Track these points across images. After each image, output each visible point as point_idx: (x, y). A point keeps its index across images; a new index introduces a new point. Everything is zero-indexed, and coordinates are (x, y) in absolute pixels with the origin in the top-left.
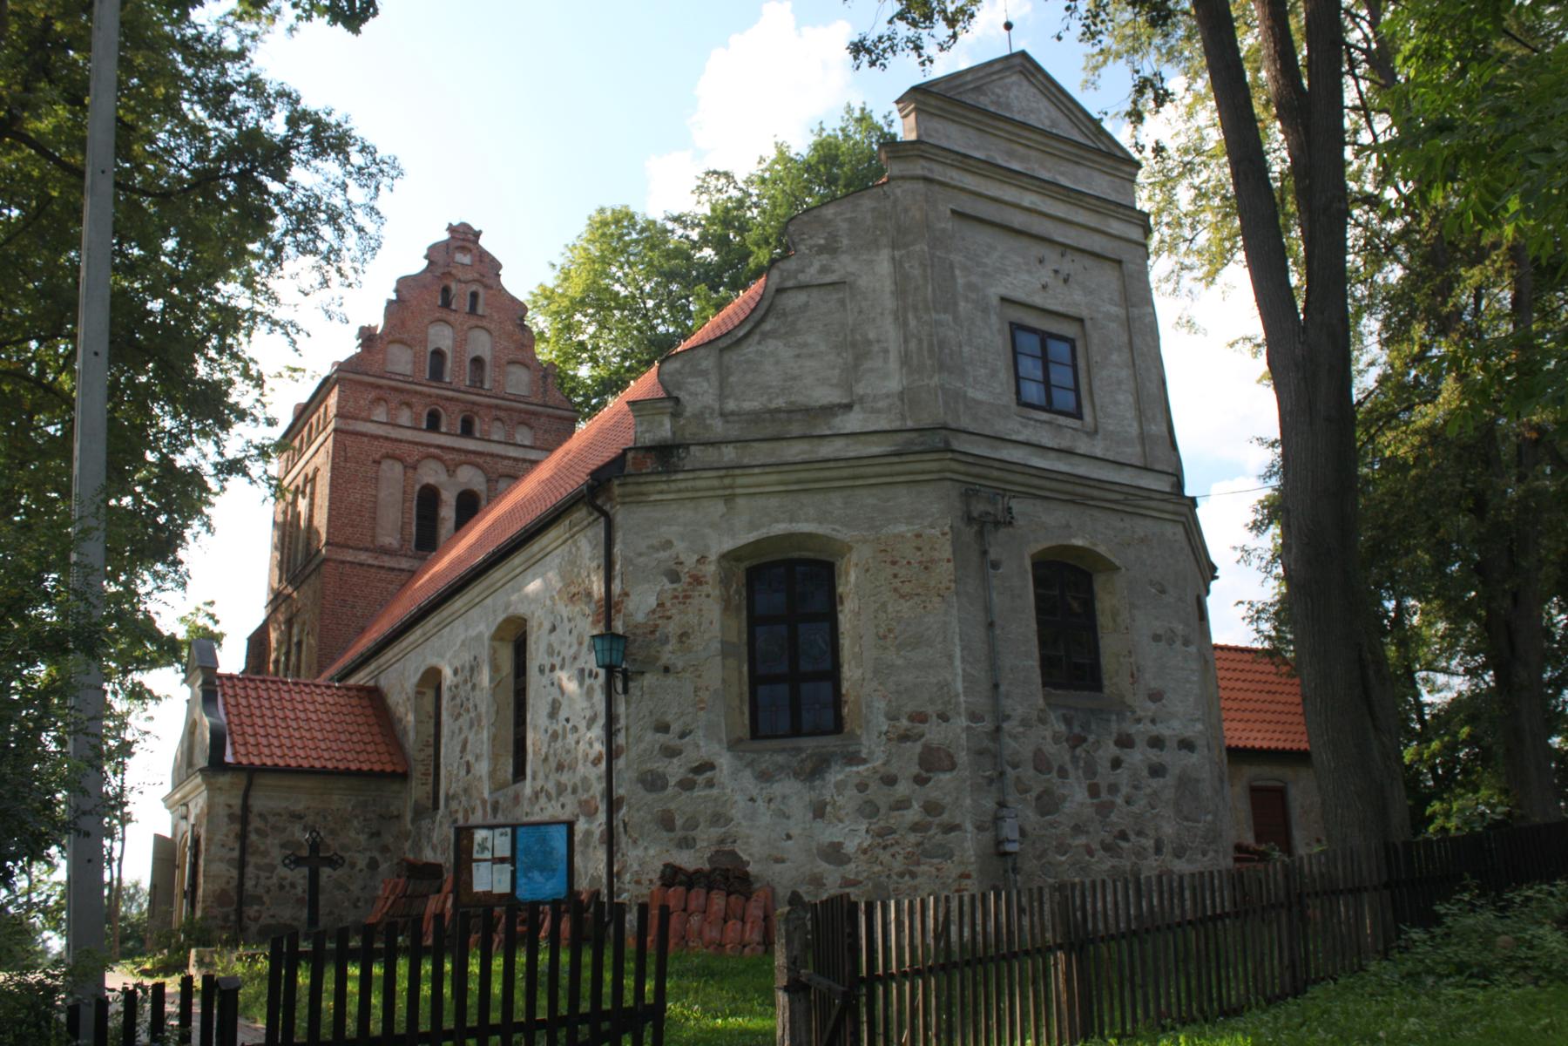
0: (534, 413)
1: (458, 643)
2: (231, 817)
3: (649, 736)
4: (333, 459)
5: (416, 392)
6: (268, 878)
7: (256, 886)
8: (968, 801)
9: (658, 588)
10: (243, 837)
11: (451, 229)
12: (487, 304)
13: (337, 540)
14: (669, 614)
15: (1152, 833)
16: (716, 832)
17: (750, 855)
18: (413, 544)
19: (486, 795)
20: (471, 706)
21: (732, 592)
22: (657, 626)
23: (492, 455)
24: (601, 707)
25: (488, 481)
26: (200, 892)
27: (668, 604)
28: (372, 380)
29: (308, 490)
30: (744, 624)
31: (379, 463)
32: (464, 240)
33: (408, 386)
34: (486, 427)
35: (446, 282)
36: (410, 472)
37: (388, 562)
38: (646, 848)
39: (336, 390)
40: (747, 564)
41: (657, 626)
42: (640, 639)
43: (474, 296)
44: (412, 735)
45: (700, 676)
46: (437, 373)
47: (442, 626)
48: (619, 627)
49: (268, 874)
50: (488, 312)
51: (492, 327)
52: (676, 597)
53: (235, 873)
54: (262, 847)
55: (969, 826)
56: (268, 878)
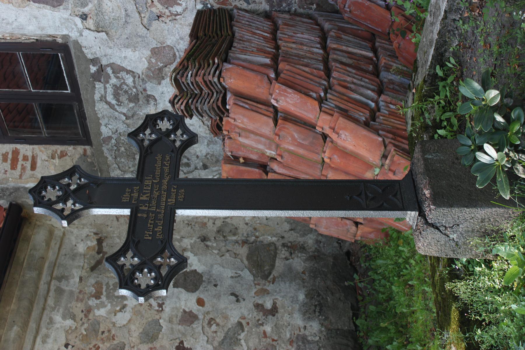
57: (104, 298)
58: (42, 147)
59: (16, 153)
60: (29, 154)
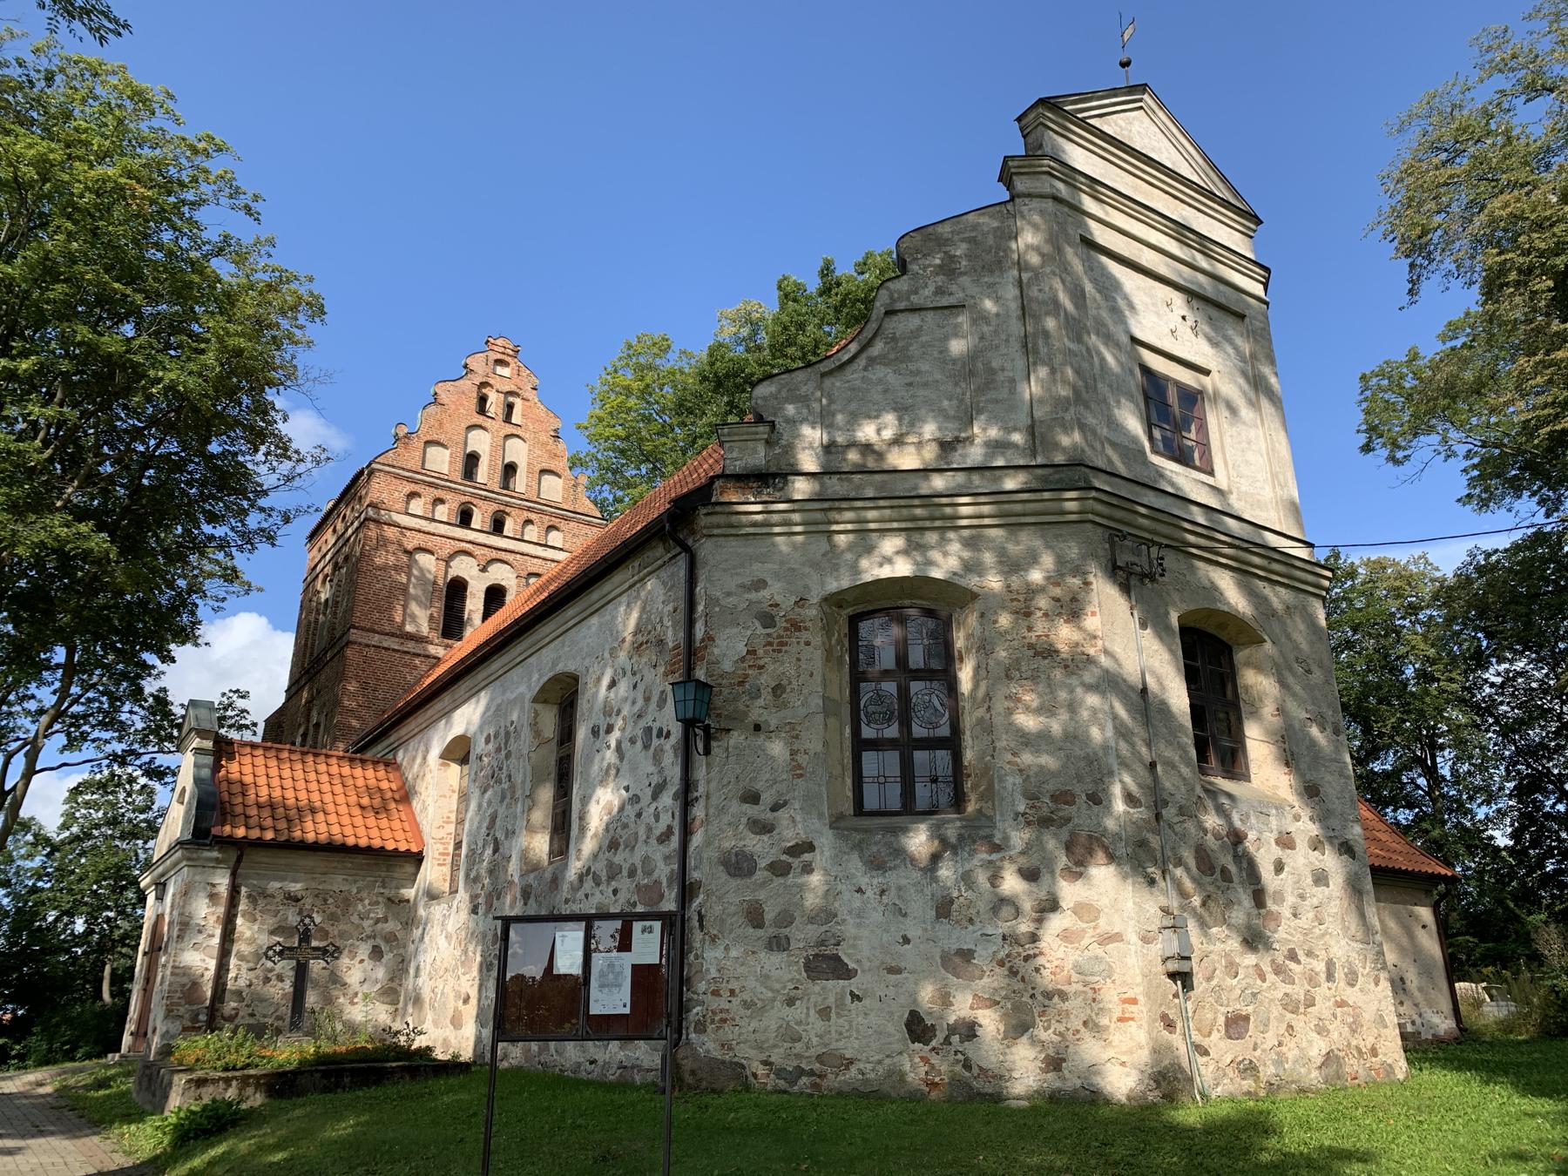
3: (735, 807)
8: (1130, 904)
9: (749, 633)
14: (761, 662)
15: (1322, 955)
16: (813, 932)
17: (858, 961)
21: (833, 642)
22: (747, 676)
24: (674, 772)
27: (761, 652)
30: (847, 678)
38: (727, 948)
40: (850, 611)
41: (747, 676)
42: (726, 691)
45: (797, 737)
48: (700, 674)
52: (770, 644)
55: (1133, 937)
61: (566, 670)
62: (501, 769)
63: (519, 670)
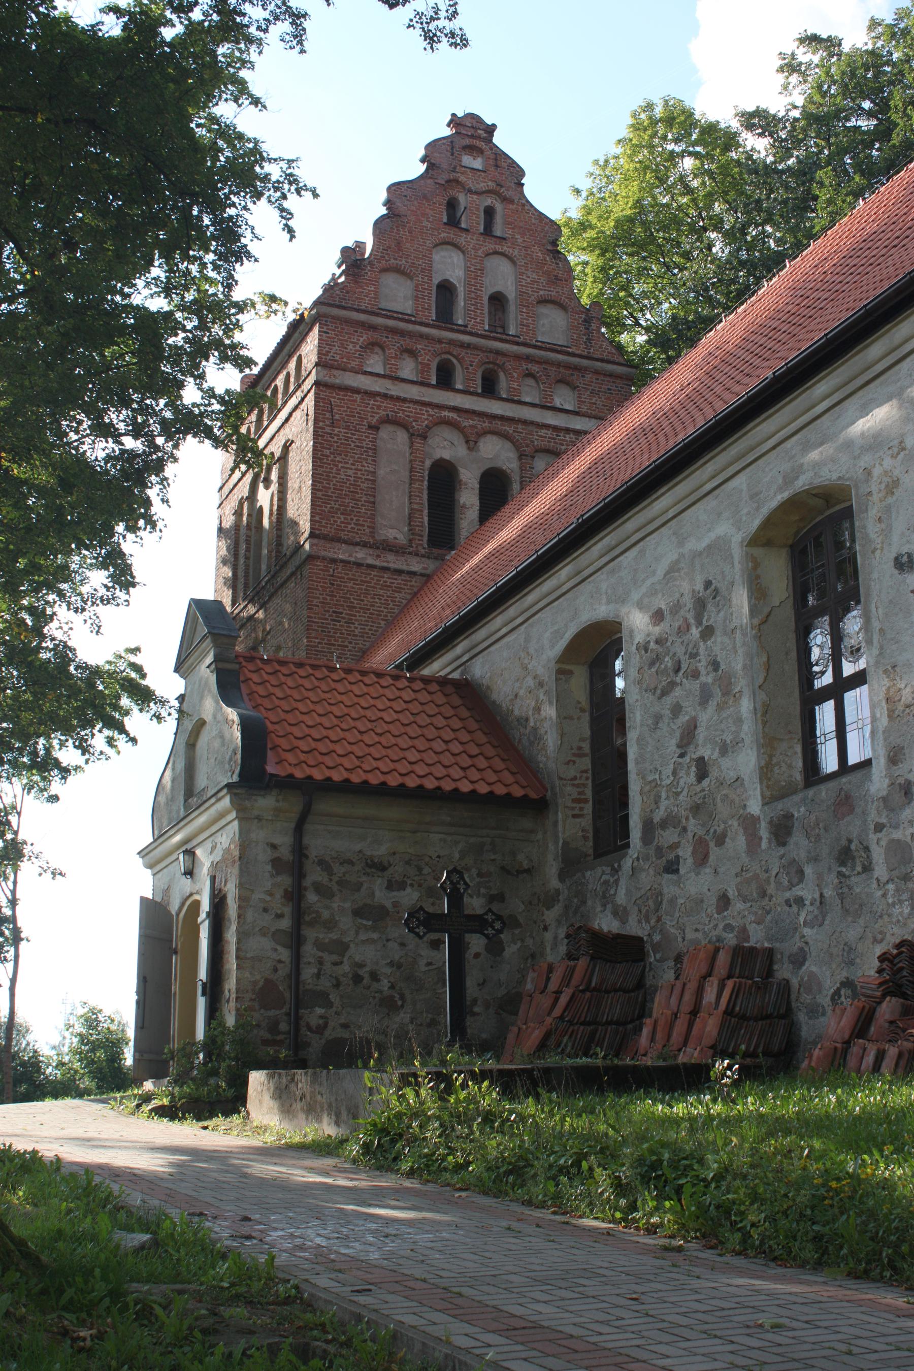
0: (576, 368)
1: (660, 573)
2: (277, 863)
4: (316, 421)
5: (422, 336)
6: (335, 964)
7: (318, 975)
10: (295, 896)
11: (455, 121)
12: (507, 223)
13: (325, 531)
18: (425, 539)
19: (755, 807)
20: (702, 666)
23: (525, 422)
25: (521, 456)
26: (231, 984)
28: (362, 317)
29: (274, 476)
31: (377, 429)
32: (472, 136)
33: (410, 327)
34: (515, 385)
35: (452, 193)
36: (418, 441)
37: (393, 561)
39: (316, 329)
43: (489, 212)
44: (551, 740)
46: (445, 315)
47: (614, 555)
49: (335, 958)
50: (508, 233)
51: (516, 252)
53: (285, 954)
54: (326, 914)
56: (335, 964)
57: (478, 880)
58: (590, 821)
59: (586, 801)
60: (585, 812)
61: (817, 482)
62: (694, 656)
63: (710, 503)
